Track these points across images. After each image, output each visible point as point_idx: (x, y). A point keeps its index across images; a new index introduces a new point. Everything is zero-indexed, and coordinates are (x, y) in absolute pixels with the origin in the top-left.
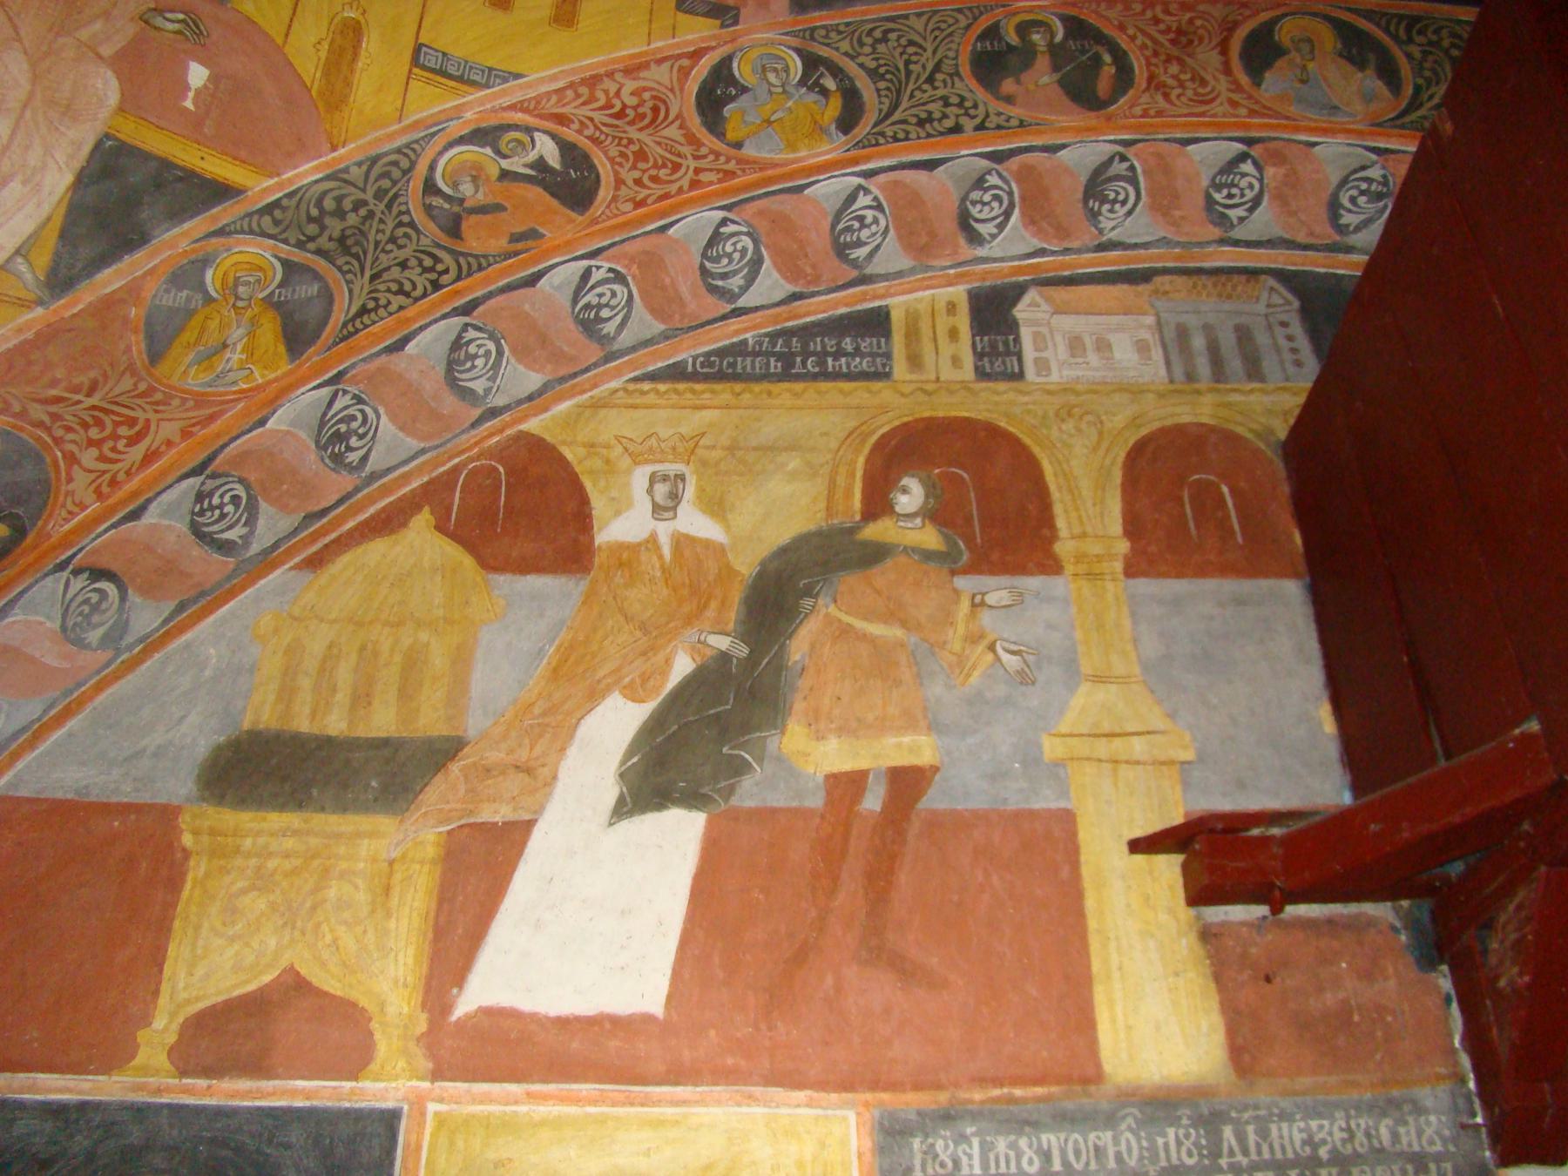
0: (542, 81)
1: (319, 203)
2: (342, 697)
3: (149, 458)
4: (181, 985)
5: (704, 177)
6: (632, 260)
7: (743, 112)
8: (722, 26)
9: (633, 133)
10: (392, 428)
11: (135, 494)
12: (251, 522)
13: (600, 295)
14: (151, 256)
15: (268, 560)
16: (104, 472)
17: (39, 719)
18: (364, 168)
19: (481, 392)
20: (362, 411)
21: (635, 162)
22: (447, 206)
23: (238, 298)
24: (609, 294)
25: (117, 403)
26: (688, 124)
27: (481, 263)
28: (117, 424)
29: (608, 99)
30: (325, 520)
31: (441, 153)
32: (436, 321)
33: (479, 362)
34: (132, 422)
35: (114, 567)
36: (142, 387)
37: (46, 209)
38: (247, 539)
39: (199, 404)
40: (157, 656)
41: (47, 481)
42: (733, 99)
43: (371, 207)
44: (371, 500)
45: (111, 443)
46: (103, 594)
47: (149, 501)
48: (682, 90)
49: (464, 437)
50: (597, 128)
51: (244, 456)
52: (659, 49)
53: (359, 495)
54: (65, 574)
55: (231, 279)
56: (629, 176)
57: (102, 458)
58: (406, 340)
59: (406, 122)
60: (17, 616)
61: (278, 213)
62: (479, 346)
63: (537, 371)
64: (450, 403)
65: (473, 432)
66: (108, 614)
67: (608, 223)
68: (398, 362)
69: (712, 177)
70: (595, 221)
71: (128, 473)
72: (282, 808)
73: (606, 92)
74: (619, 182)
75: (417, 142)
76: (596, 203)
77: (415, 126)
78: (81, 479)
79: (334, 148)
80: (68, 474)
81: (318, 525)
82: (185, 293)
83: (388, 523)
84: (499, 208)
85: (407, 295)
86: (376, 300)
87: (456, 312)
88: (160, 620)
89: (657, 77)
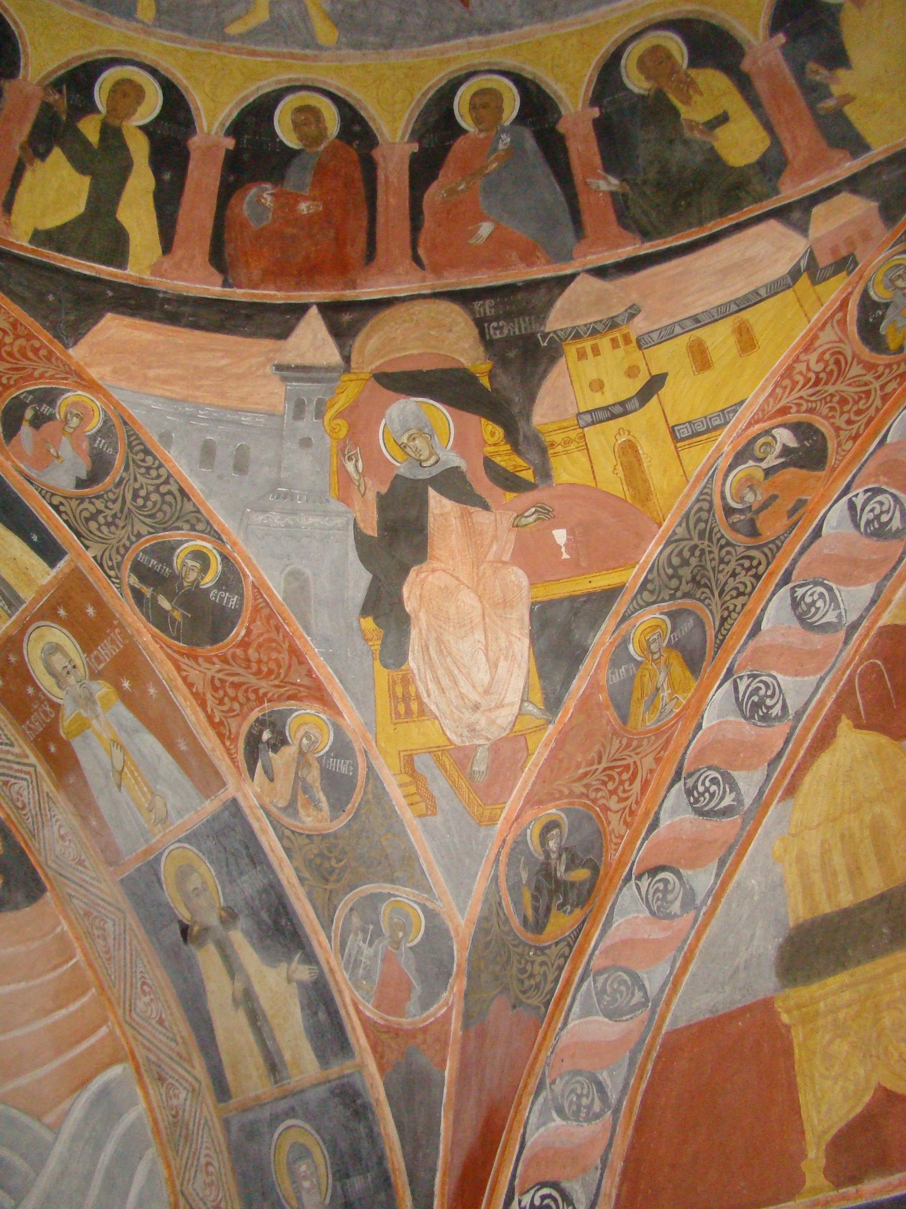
0: (757, 396)
1: (670, 565)
2: (842, 877)
3: (645, 784)
4: (816, 1122)
5: (889, 389)
6: (877, 475)
7: (893, 322)
8: (849, 273)
9: (831, 389)
10: (789, 678)
11: (646, 814)
12: (734, 787)
13: (872, 510)
14: (594, 657)
15: (762, 804)
16: (624, 809)
17: (671, 973)
18: (684, 525)
19: (835, 620)
20: (761, 681)
21: (841, 408)
22: (742, 517)
23: (653, 653)
24: (877, 506)
25: (616, 760)
26: (862, 357)
27: (777, 545)
28: (620, 774)
29: (805, 376)
30: (784, 759)
31: (723, 484)
32: (770, 599)
33: (819, 604)
34: (626, 768)
35: (661, 862)
36: (624, 741)
37: (524, 667)
38: (739, 800)
39: (657, 736)
40: (723, 900)
41: (599, 831)
42: (882, 318)
43: (701, 547)
44: (807, 729)
45: (621, 788)
46: (666, 881)
47: (657, 814)
48: (847, 336)
49: (844, 654)
50: (808, 401)
51: (701, 752)
52: (818, 320)
53: (797, 731)
54: (633, 882)
55: (645, 644)
56: (841, 422)
57: (621, 800)
58: (758, 624)
59: (692, 480)
60: (618, 921)
61: (650, 586)
62: (812, 595)
63: (865, 583)
64: (817, 640)
65: (849, 647)
66: (676, 890)
67: (842, 465)
68: (763, 639)
69: (893, 385)
70: (833, 469)
71: (637, 803)
72: (834, 972)
73: (801, 373)
74: (838, 429)
75: (705, 487)
76: (829, 456)
77: (699, 478)
78: (614, 818)
79: (660, 525)
80: (607, 819)
81: (782, 764)
82: (623, 669)
83: (825, 738)
84: (774, 497)
85: (743, 594)
86: (727, 608)
87: (779, 586)
88: (713, 877)
89: (827, 340)
